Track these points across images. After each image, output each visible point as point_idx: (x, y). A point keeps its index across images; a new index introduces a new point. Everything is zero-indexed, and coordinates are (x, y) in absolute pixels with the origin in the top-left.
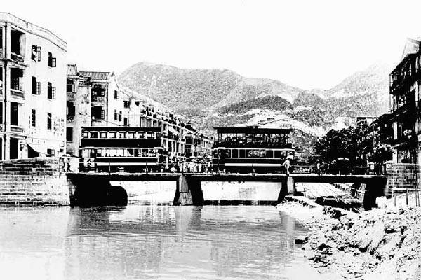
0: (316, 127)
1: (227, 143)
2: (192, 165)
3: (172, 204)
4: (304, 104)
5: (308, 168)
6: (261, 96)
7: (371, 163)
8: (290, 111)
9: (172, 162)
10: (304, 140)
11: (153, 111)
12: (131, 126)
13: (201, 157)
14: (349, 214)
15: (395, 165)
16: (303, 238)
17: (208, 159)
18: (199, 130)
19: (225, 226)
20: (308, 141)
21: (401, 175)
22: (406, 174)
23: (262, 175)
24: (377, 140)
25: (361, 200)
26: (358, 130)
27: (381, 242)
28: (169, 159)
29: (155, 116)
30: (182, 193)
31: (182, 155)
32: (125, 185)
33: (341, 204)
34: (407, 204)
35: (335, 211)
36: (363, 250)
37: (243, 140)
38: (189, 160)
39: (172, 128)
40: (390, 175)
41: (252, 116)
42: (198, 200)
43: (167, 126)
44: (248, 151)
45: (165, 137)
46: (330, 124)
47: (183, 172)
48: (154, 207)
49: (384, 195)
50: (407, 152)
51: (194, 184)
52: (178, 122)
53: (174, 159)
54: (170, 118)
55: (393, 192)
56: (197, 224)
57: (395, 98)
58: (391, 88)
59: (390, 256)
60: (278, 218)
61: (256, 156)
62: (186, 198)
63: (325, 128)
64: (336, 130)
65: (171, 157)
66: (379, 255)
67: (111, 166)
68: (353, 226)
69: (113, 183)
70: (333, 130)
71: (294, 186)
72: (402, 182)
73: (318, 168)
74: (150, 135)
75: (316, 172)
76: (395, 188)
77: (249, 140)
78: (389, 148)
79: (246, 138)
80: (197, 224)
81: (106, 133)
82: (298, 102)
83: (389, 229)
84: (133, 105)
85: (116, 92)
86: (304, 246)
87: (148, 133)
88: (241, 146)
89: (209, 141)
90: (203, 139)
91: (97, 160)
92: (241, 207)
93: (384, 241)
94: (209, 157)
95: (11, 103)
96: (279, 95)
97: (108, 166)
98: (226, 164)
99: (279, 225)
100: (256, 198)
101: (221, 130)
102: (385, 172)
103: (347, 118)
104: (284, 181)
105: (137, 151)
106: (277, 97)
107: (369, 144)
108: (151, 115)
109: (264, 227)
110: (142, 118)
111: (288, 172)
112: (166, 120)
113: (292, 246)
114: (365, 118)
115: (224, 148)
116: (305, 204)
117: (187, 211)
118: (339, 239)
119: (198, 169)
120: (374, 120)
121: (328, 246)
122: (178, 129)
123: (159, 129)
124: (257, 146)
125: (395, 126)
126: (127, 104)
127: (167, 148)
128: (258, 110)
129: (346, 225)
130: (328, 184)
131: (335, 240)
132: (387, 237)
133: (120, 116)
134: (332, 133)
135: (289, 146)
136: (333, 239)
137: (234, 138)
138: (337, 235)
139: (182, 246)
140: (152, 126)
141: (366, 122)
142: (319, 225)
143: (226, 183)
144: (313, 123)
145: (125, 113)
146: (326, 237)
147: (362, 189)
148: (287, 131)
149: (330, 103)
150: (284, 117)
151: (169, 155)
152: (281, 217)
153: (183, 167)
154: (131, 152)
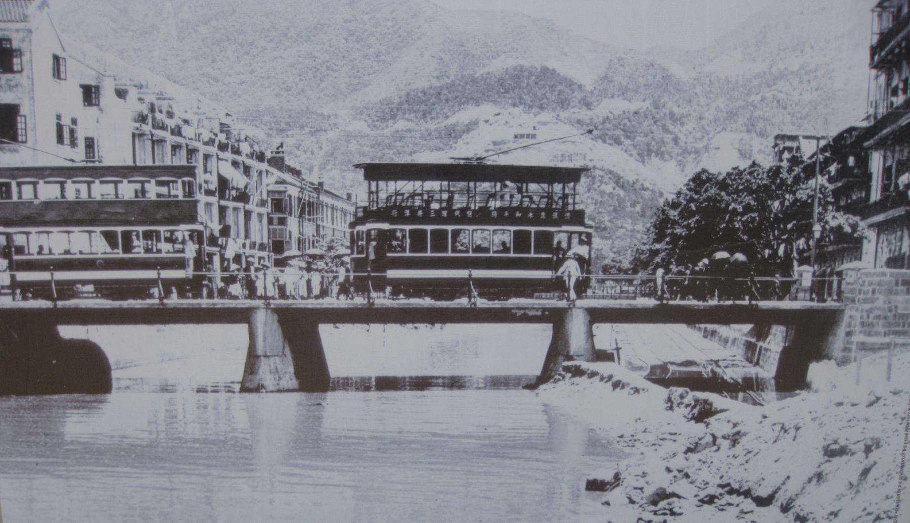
0: (655, 160)
1: (391, 212)
2: (293, 277)
3: (237, 387)
4: (623, 92)
5: (630, 282)
6: (496, 67)
7: (805, 267)
8: (584, 114)
9: (234, 266)
10: (621, 201)
11: (170, 115)
12: (107, 163)
13: (317, 251)
14: (732, 409)
15: (867, 274)
16: (606, 475)
17: (339, 257)
18: (311, 170)
19: (392, 446)
20: (633, 205)
21: (881, 300)
22: (893, 298)
23: (497, 304)
24: (824, 205)
25: (768, 370)
26: (775, 172)
27: (810, 480)
28: (223, 259)
29: (177, 132)
30: (266, 356)
31: (262, 247)
32: (101, 335)
33: (716, 384)
34: (888, 378)
35: (697, 401)
36: (763, 502)
37: (440, 201)
38: (281, 263)
39: (229, 165)
40: (853, 301)
41: (470, 127)
42: (313, 376)
43: (214, 159)
44: (456, 233)
45: (209, 193)
46: (697, 152)
47: (265, 298)
48: (186, 399)
49: (830, 358)
50: (901, 239)
51: (300, 330)
52: (245, 148)
53: (237, 258)
54: (222, 137)
55: (854, 347)
56: (309, 443)
57: (883, 79)
58: (874, 50)
59: (832, 513)
60: (540, 421)
61: (478, 249)
62: (278, 368)
63: (682, 165)
64: (713, 170)
65: (230, 254)
66: (801, 514)
67: (59, 283)
68: (743, 441)
69: (68, 332)
70: (704, 171)
71: (590, 335)
72: (881, 322)
73: (659, 281)
74: (164, 190)
75: (651, 294)
76: (858, 338)
77: (460, 202)
78: (854, 227)
79: (451, 194)
80: (309, 443)
81: (35, 184)
82: (607, 85)
83: (834, 447)
84: (108, 96)
85: (56, 59)
86: (609, 496)
87: (160, 184)
88: (438, 219)
89: (339, 204)
90: (324, 198)
91: (15, 266)
92: (435, 394)
93: (819, 476)
94: (342, 251)
95: (18, 105)
96: (551, 65)
97: (47, 284)
98: (392, 274)
99: (546, 443)
100: (476, 368)
101: (375, 172)
102: (840, 293)
103: (746, 137)
104: (557, 319)
105: (127, 236)
106: (545, 70)
107: (801, 213)
108: (163, 127)
109: (496, 448)
110: (137, 136)
111: (573, 295)
112: (211, 142)
113: (575, 496)
114: (794, 138)
115: (386, 226)
116: (616, 385)
117: (283, 407)
118: (704, 475)
119: (309, 290)
120: (823, 143)
121: (674, 495)
122: (247, 170)
123: (190, 171)
124: (483, 217)
125: (876, 162)
126: (90, 94)
127: (216, 227)
128: (486, 110)
129: (724, 437)
130: (681, 328)
131: (693, 477)
132: (827, 468)
133: (72, 132)
134: (700, 181)
135: (578, 217)
136: (687, 476)
137: (413, 195)
138: (699, 464)
139: (271, 501)
140: (168, 162)
141: (798, 149)
142: (651, 438)
143: (393, 328)
144: (650, 152)
145: (88, 122)
146: (669, 470)
147: (776, 341)
148: (571, 175)
149: (699, 89)
150: (565, 129)
151: (223, 247)
152: (551, 422)
153: (265, 283)
154: (110, 237)
